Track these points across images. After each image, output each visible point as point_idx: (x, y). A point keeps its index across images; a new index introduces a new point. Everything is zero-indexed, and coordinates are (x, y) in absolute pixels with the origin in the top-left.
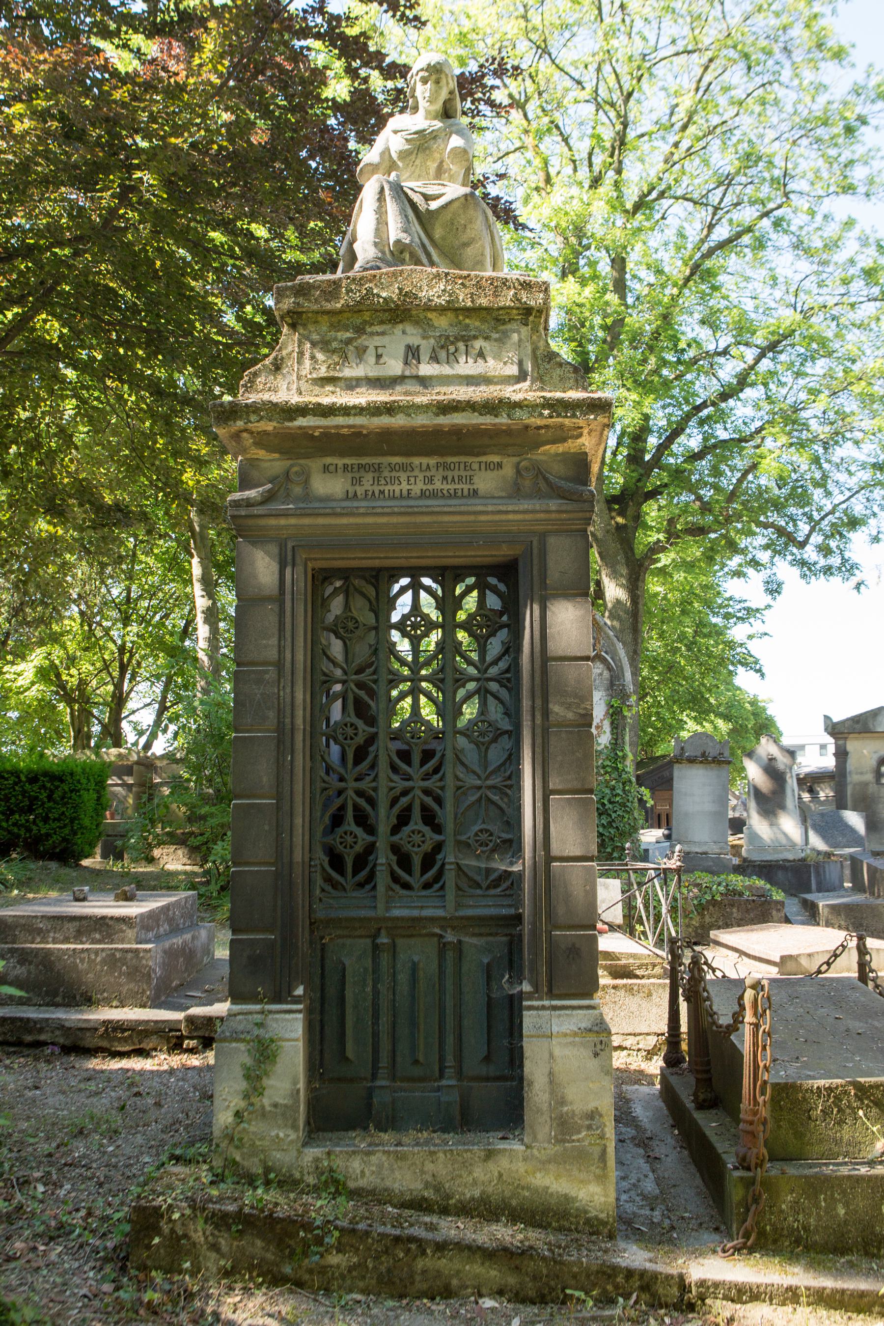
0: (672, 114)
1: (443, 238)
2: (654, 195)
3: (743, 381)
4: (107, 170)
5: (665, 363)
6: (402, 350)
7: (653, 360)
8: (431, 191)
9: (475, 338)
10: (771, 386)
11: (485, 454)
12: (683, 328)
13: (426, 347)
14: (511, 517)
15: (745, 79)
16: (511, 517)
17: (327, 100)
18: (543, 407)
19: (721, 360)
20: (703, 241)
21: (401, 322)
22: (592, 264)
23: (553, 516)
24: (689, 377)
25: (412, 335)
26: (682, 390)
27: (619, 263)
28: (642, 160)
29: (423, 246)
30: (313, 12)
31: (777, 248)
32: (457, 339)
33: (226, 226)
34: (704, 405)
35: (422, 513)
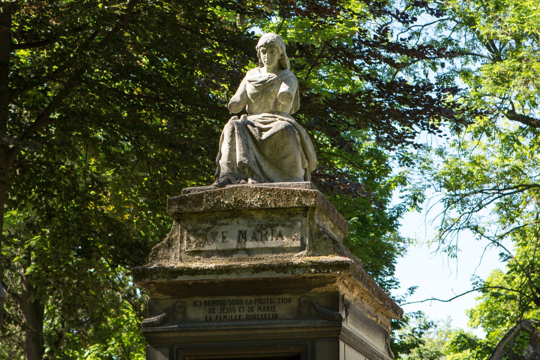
9: (277, 225)
11: (281, 293)
13: (250, 231)
14: (295, 330)
16: (295, 330)
18: (312, 267)
21: (237, 217)
23: (319, 330)
25: (241, 225)
35: (246, 329)
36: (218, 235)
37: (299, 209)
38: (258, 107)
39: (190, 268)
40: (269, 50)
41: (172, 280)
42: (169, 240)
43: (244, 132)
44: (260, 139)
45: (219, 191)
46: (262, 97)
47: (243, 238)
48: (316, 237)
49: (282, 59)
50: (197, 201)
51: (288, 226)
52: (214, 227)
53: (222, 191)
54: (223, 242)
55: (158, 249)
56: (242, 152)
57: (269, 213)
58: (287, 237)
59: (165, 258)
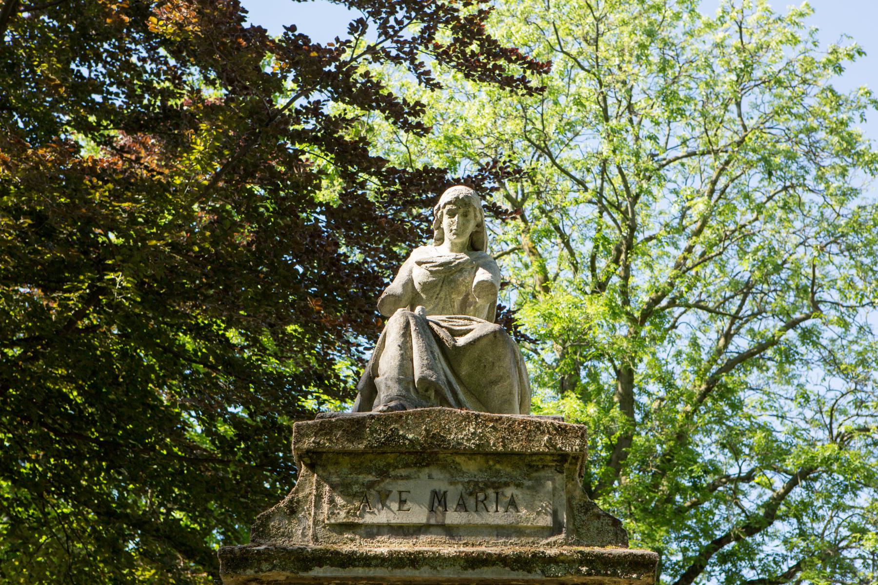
0: (683, 216)
1: (470, 376)
2: (664, 303)
3: (771, 512)
4: (77, 269)
5: (677, 488)
6: (427, 496)
7: (665, 486)
8: (459, 324)
9: (506, 485)
10: (805, 519)
12: (699, 450)
13: (453, 492)
15: (766, 183)
17: (321, 204)
18: (581, 563)
19: (744, 486)
20: (719, 352)
21: (428, 465)
22: (594, 376)
24: (706, 505)
25: (437, 480)
26: (699, 521)
27: (626, 376)
28: (650, 266)
29: (449, 383)
30: (307, 113)
31: (807, 363)
32: (487, 486)
33: (197, 331)
34: (726, 539)
36: (391, 496)
37: (549, 458)
38: (432, 306)
39: (337, 553)
40: (461, 210)
41: (301, 574)
42: (291, 501)
43: (425, 331)
44: (454, 346)
45: (397, 415)
46: (441, 290)
47: (440, 504)
48: (579, 512)
49: (476, 232)
50: (353, 432)
51: (528, 488)
52: (383, 481)
53: (401, 416)
54: (400, 510)
55: (269, 518)
56: (425, 362)
57: (491, 463)
58: (526, 508)
59: (283, 536)
